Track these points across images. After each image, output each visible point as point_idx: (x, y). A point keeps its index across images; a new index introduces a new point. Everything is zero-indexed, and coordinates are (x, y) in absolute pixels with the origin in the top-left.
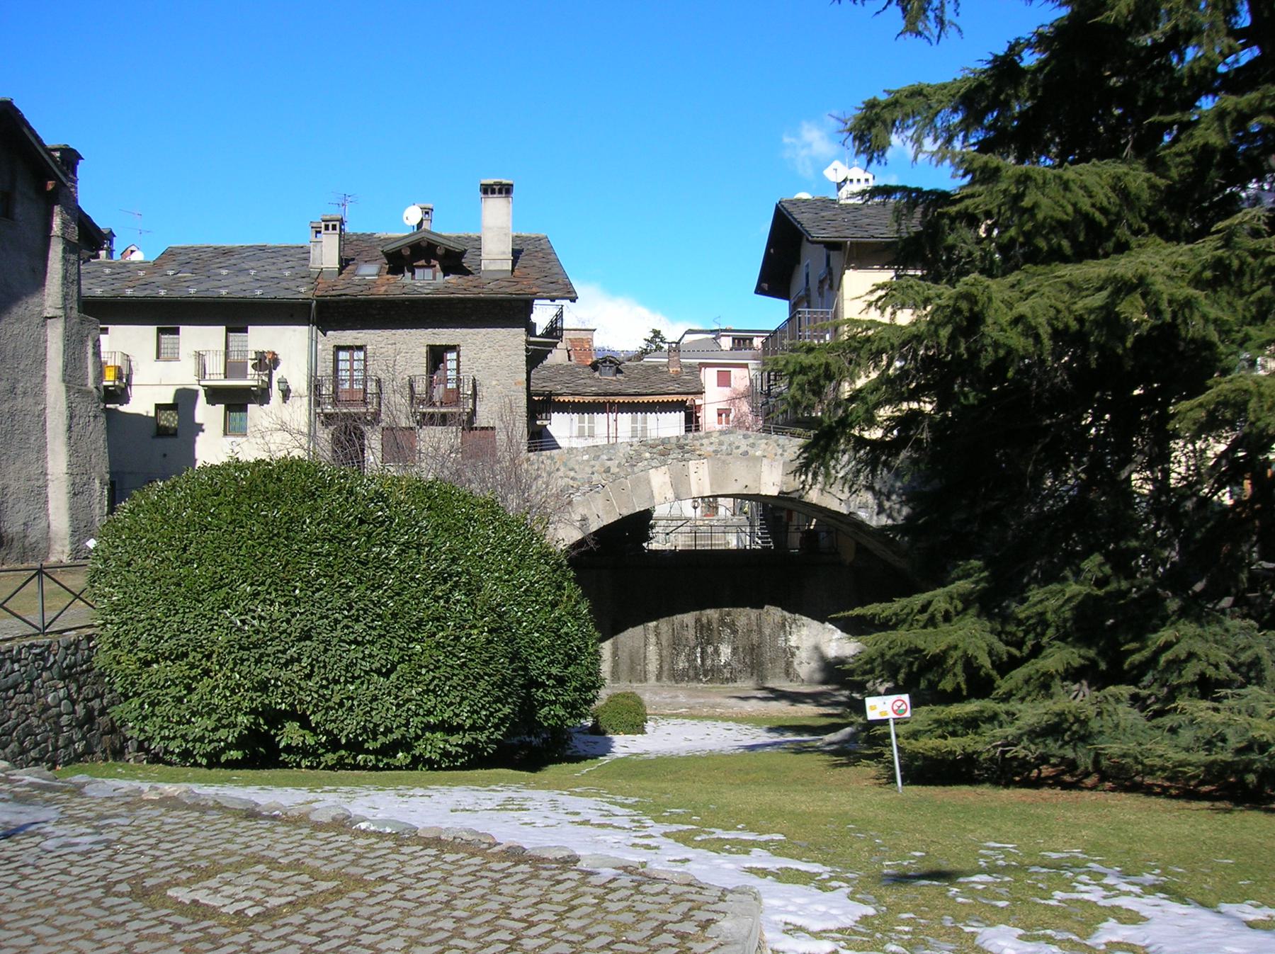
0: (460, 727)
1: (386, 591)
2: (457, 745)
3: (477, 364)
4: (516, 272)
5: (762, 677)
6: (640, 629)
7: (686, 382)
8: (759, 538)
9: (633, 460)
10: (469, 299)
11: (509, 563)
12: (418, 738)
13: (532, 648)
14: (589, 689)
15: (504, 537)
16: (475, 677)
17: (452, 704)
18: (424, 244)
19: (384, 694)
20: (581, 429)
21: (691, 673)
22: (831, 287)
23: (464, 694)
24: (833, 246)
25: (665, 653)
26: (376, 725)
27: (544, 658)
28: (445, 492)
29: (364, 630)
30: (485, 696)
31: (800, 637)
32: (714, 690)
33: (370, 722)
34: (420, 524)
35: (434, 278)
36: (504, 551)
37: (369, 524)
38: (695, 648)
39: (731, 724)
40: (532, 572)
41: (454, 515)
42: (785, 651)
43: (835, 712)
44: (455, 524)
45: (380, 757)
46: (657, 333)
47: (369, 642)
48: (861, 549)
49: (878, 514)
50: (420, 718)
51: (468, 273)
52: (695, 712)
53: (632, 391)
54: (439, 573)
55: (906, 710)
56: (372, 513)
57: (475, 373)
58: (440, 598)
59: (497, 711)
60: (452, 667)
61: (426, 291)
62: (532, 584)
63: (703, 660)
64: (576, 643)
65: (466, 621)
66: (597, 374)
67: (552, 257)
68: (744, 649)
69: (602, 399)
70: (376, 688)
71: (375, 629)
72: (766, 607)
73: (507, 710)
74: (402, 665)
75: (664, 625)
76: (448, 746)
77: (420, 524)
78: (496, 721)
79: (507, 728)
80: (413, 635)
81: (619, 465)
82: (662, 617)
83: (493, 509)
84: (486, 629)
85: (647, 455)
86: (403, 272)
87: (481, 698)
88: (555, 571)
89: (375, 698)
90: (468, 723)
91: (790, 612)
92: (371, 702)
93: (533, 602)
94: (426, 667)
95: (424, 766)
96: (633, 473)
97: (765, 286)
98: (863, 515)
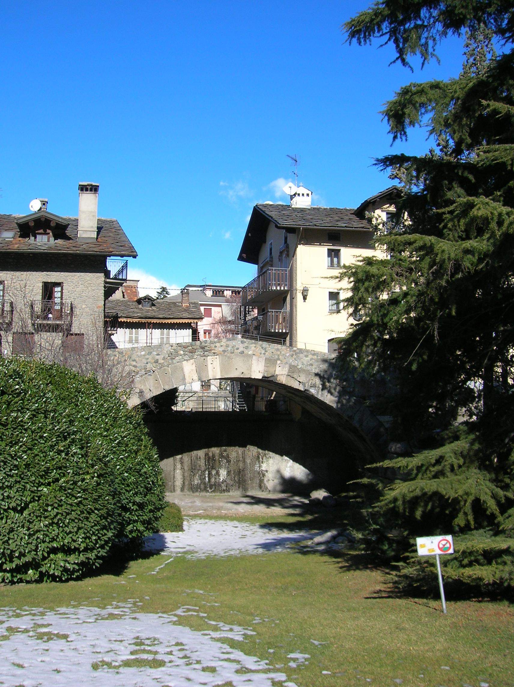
0: (76, 550)
1: (21, 446)
2: (75, 563)
3: (73, 295)
4: (99, 240)
5: (245, 489)
6: (171, 459)
7: (193, 312)
8: (238, 404)
9: (172, 355)
10: (70, 254)
11: (107, 423)
12: (44, 558)
13: (123, 484)
14: (158, 509)
15: (102, 405)
16: (88, 512)
17: (70, 532)
18: (43, 219)
19: (19, 526)
20: (131, 338)
21: (202, 486)
22: (288, 255)
23: (81, 525)
24: (291, 230)
25: (186, 474)
26: (12, 551)
27: (131, 491)
28: (61, 373)
29: (4, 477)
30: (95, 525)
31: (268, 465)
32: (217, 497)
33: (8, 549)
34: (47, 395)
35: (48, 241)
36: (103, 415)
37: (9, 395)
38: (204, 471)
39: (236, 523)
40: (122, 430)
41: (68, 389)
42: (259, 473)
43: (295, 512)
44: (69, 395)
45: (15, 574)
46: (164, 289)
47: (7, 486)
48: (305, 412)
49: (322, 390)
50: (46, 544)
51: (69, 238)
52: (209, 513)
53: (161, 316)
54: (61, 433)
55: (450, 548)
56: (11, 387)
57: (73, 300)
58: (62, 451)
59: (103, 536)
60: (71, 505)
61: (43, 248)
62: (123, 438)
63: (209, 479)
64: (152, 479)
65: (81, 469)
66: (140, 306)
67: (121, 231)
68: (234, 472)
69: (143, 321)
70: (13, 522)
71: (12, 476)
72: (248, 446)
73: (110, 534)
74: (33, 504)
75: (186, 457)
76: (67, 565)
77: (47, 395)
78: (103, 543)
79: (110, 547)
80: (42, 481)
81: (164, 358)
82: (185, 452)
83: (93, 383)
84: (96, 475)
85: (182, 352)
86: (29, 237)
87: (92, 527)
88: (136, 428)
89: (12, 530)
90: (83, 546)
91: (262, 449)
92: (9, 534)
93: (123, 451)
94: (52, 505)
95: (48, 578)
96: (173, 363)
97: (244, 255)
98: (313, 391)
